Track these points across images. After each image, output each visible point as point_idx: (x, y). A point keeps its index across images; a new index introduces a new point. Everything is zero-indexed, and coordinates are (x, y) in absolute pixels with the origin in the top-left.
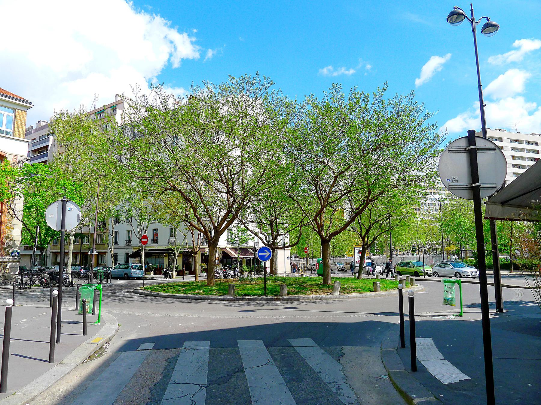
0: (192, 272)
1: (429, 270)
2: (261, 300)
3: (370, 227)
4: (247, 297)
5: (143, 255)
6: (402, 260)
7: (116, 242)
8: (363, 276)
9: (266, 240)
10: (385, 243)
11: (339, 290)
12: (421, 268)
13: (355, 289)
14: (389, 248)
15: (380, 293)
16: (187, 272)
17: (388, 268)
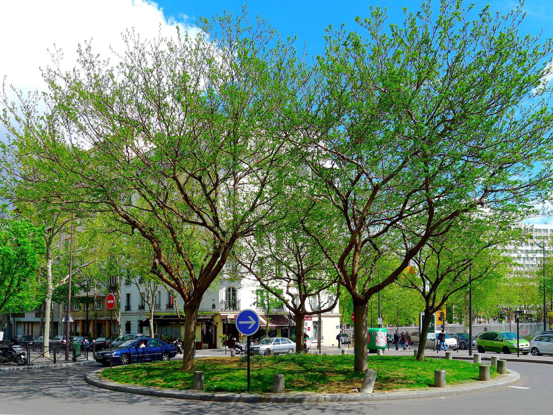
0: (213, 346)
1: (524, 344)
2: (239, 400)
3: (438, 281)
4: (218, 395)
5: (152, 324)
6: (485, 329)
7: (128, 308)
8: (427, 352)
9: (293, 302)
10: (464, 308)
11: (373, 383)
12: (514, 343)
13: (404, 382)
14: (468, 316)
15: (446, 388)
16: (207, 345)
17: (465, 343)
